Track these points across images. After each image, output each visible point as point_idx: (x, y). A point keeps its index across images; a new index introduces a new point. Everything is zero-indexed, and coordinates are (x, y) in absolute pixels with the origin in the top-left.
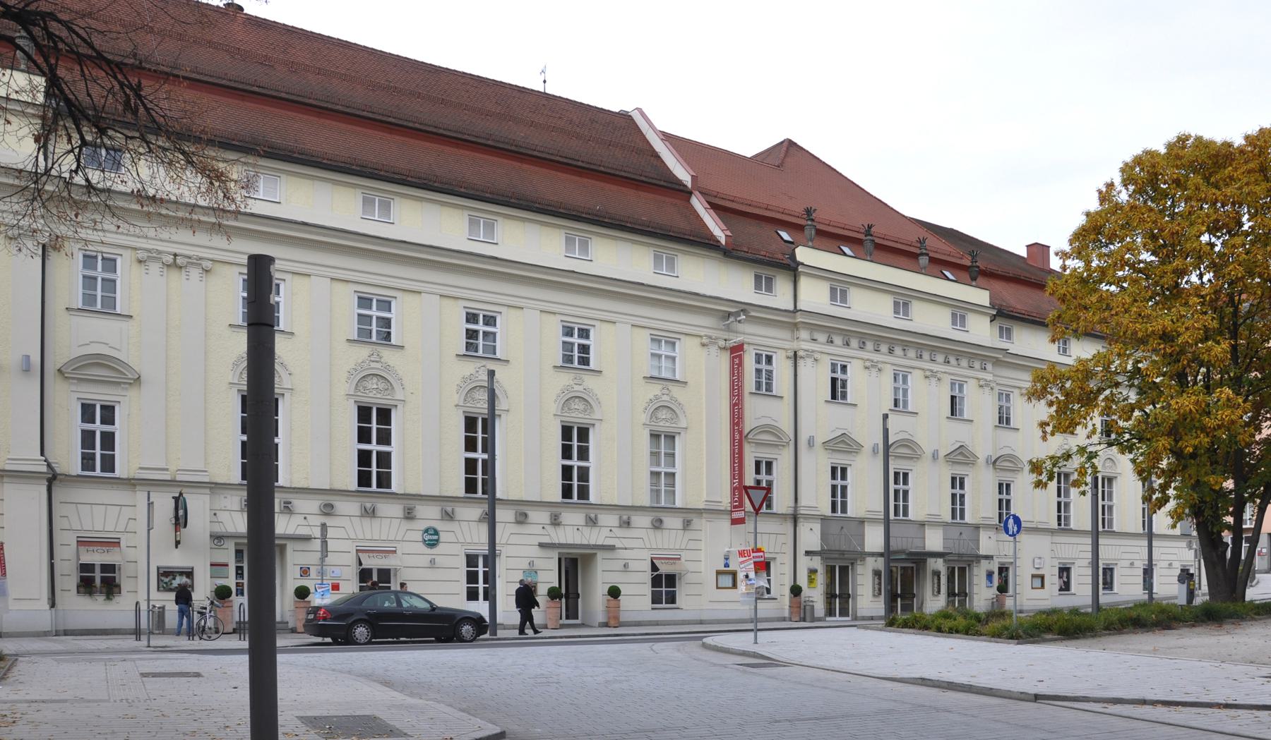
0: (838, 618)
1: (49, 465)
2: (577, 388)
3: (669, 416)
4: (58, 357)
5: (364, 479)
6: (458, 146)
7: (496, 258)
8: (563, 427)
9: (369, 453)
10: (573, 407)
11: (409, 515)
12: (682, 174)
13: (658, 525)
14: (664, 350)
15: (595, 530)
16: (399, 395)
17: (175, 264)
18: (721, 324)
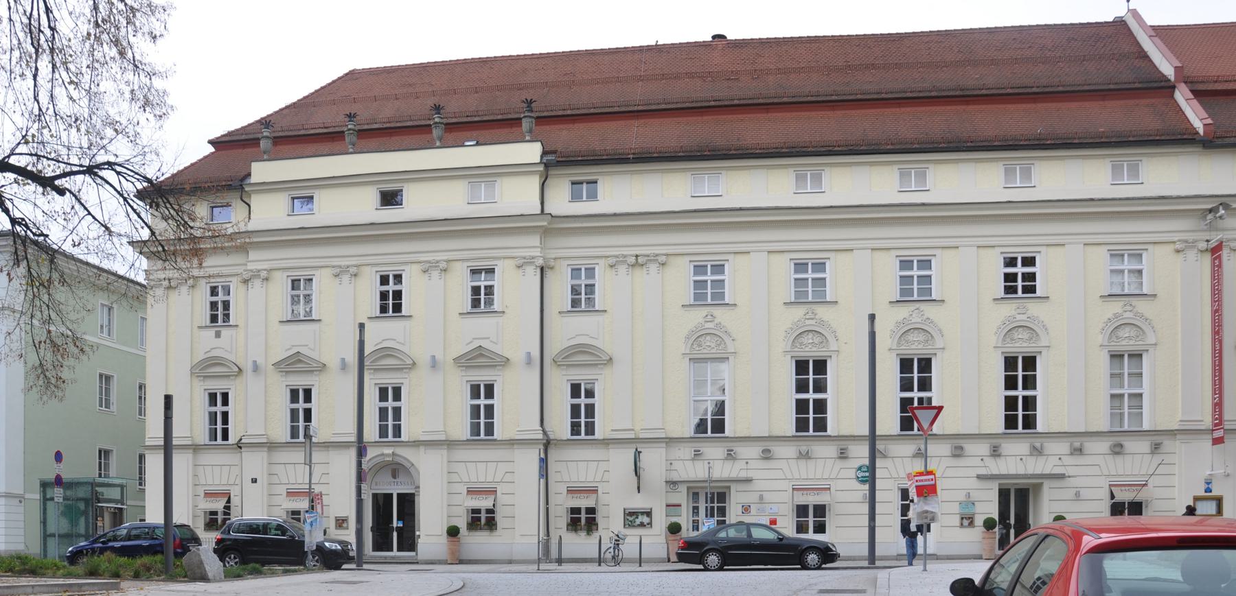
0: (395, 553)
1: (545, 432)
2: (1019, 317)
3: (1133, 334)
4: (553, 349)
5: (801, 425)
6: (900, 106)
7: (1092, 200)
8: (1006, 359)
9: (579, 406)
10: (1016, 336)
11: (843, 455)
12: (1167, 69)
13: (1118, 450)
14: (1127, 265)
15: (1041, 460)
16: (833, 346)
17: (638, 263)
18: (1202, 225)
